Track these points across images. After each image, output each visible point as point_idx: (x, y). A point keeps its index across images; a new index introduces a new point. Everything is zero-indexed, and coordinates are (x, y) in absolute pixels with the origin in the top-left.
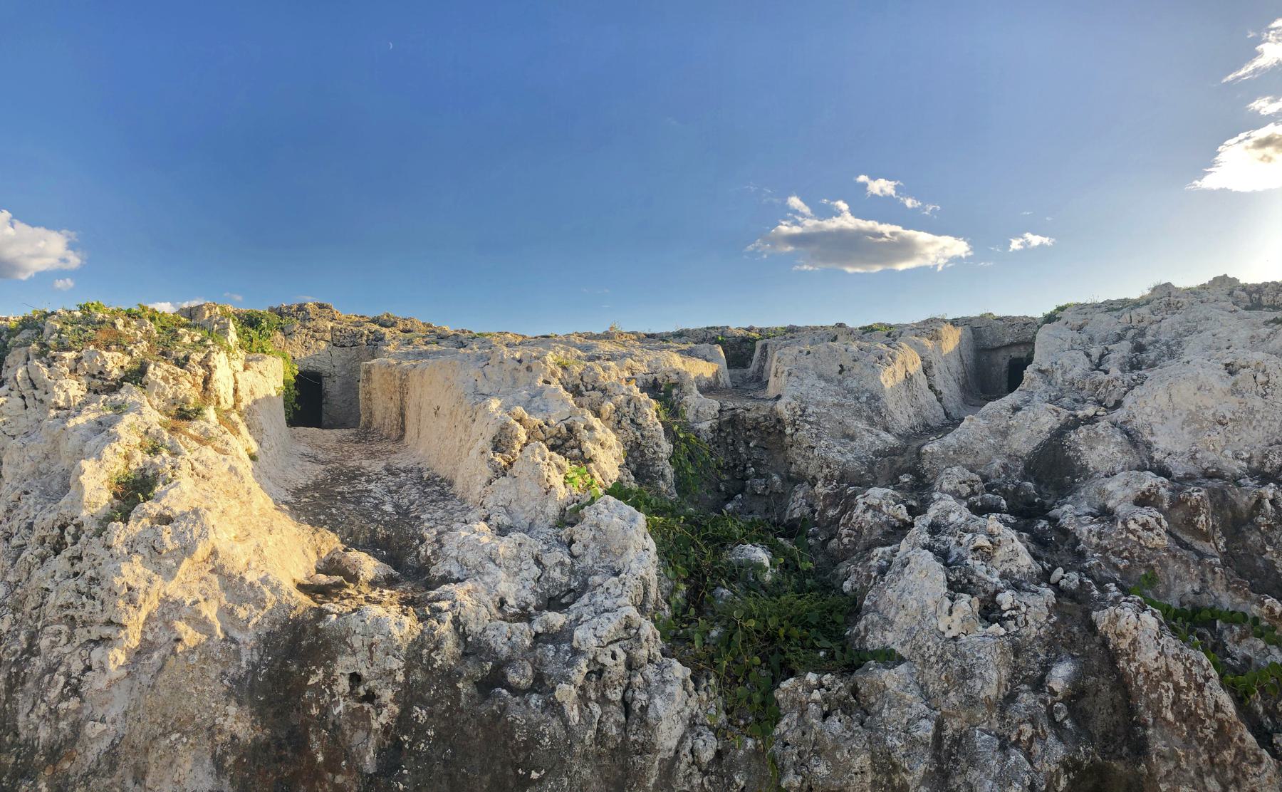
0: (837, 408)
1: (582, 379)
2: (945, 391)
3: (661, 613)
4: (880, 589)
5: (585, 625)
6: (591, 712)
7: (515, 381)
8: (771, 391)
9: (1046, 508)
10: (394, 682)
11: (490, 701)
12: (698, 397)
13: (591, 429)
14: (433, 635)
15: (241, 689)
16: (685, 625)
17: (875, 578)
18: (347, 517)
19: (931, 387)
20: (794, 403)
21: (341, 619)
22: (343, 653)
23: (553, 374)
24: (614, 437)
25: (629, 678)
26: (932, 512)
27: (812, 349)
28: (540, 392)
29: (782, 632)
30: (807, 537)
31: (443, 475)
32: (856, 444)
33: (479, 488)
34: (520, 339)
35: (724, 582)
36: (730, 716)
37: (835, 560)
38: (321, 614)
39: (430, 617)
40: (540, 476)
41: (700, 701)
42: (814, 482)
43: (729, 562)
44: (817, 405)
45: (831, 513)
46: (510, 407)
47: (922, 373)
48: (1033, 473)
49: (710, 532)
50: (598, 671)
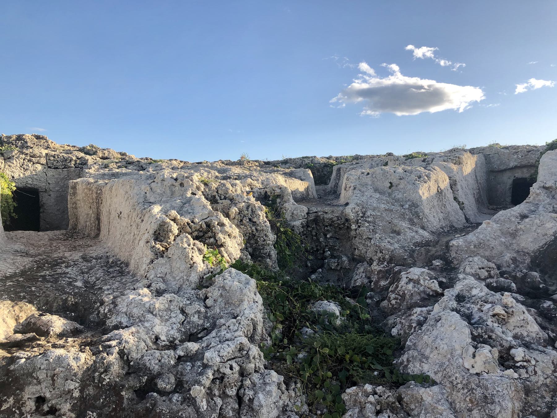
0: (388, 212)
1: (217, 192)
2: (466, 202)
3: (265, 342)
4: (418, 335)
5: (212, 349)
6: (215, 403)
7: (173, 193)
8: (342, 200)
9: (550, 292)
10: (72, 398)
11: (145, 401)
12: (293, 204)
13: (222, 225)
14: (103, 363)
16: (281, 350)
17: (415, 328)
18: (44, 292)
19: (455, 199)
20: (357, 208)
21: (29, 361)
22: (30, 384)
23: (198, 188)
24: (237, 230)
25: (242, 381)
26: (458, 287)
27: (371, 171)
28: (189, 201)
29: (348, 357)
30: (366, 298)
31: (122, 259)
32: (401, 237)
33: (144, 266)
34: (182, 164)
35: (308, 324)
36: (310, 408)
37: (385, 314)
38: (13, 360)
39: (102, 351)
40: (187, 256)
41: (290, 397)
42: (371, 262)
43: (312, 312)
44: (374, 210)
45: (383, 283)
46: (168, 210)
47: (449, 189)
48: (538, 265)
49: (300, 292)
50: (220, 378)
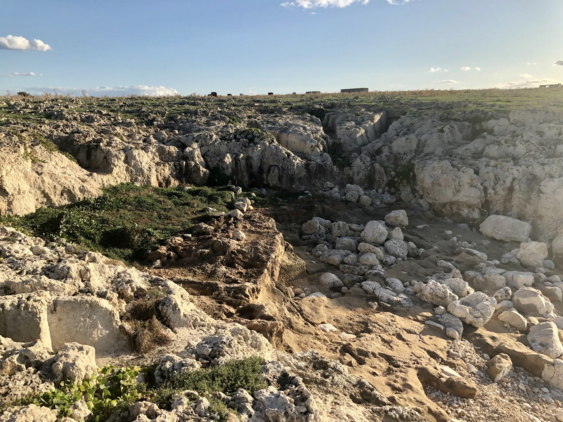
15: (305, 168)
